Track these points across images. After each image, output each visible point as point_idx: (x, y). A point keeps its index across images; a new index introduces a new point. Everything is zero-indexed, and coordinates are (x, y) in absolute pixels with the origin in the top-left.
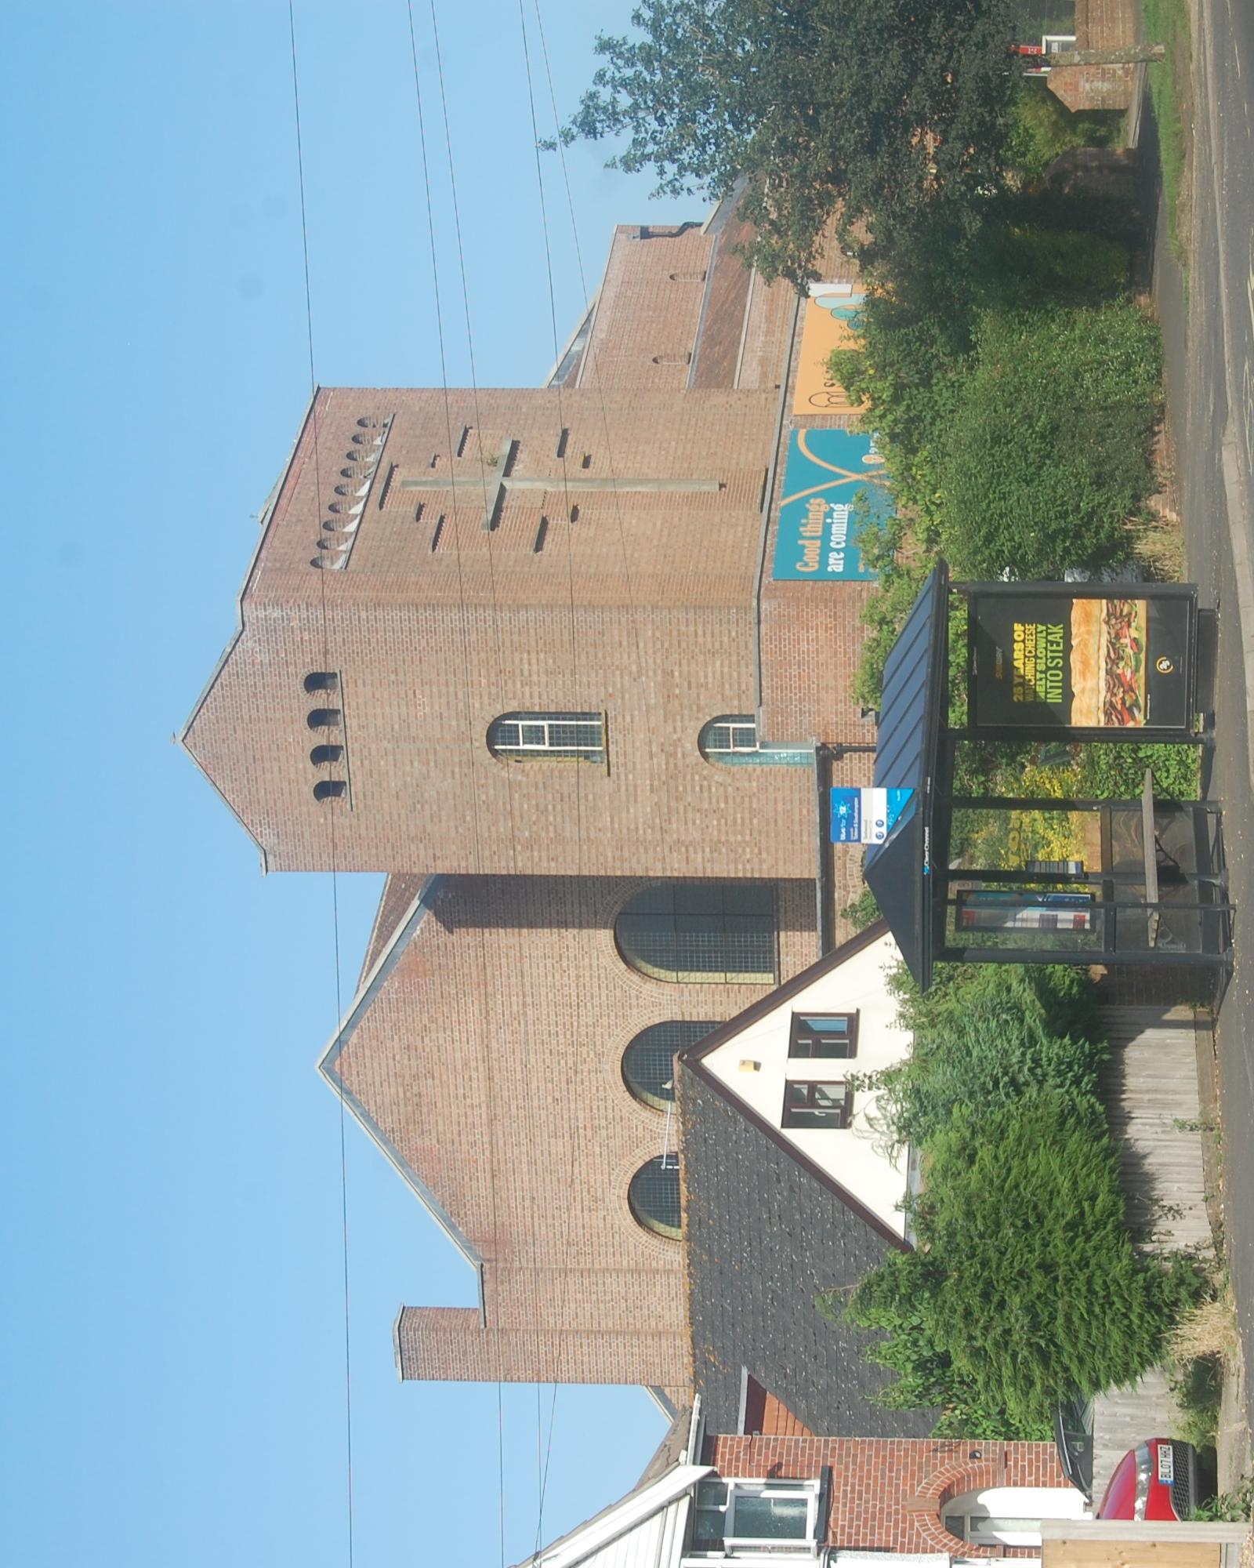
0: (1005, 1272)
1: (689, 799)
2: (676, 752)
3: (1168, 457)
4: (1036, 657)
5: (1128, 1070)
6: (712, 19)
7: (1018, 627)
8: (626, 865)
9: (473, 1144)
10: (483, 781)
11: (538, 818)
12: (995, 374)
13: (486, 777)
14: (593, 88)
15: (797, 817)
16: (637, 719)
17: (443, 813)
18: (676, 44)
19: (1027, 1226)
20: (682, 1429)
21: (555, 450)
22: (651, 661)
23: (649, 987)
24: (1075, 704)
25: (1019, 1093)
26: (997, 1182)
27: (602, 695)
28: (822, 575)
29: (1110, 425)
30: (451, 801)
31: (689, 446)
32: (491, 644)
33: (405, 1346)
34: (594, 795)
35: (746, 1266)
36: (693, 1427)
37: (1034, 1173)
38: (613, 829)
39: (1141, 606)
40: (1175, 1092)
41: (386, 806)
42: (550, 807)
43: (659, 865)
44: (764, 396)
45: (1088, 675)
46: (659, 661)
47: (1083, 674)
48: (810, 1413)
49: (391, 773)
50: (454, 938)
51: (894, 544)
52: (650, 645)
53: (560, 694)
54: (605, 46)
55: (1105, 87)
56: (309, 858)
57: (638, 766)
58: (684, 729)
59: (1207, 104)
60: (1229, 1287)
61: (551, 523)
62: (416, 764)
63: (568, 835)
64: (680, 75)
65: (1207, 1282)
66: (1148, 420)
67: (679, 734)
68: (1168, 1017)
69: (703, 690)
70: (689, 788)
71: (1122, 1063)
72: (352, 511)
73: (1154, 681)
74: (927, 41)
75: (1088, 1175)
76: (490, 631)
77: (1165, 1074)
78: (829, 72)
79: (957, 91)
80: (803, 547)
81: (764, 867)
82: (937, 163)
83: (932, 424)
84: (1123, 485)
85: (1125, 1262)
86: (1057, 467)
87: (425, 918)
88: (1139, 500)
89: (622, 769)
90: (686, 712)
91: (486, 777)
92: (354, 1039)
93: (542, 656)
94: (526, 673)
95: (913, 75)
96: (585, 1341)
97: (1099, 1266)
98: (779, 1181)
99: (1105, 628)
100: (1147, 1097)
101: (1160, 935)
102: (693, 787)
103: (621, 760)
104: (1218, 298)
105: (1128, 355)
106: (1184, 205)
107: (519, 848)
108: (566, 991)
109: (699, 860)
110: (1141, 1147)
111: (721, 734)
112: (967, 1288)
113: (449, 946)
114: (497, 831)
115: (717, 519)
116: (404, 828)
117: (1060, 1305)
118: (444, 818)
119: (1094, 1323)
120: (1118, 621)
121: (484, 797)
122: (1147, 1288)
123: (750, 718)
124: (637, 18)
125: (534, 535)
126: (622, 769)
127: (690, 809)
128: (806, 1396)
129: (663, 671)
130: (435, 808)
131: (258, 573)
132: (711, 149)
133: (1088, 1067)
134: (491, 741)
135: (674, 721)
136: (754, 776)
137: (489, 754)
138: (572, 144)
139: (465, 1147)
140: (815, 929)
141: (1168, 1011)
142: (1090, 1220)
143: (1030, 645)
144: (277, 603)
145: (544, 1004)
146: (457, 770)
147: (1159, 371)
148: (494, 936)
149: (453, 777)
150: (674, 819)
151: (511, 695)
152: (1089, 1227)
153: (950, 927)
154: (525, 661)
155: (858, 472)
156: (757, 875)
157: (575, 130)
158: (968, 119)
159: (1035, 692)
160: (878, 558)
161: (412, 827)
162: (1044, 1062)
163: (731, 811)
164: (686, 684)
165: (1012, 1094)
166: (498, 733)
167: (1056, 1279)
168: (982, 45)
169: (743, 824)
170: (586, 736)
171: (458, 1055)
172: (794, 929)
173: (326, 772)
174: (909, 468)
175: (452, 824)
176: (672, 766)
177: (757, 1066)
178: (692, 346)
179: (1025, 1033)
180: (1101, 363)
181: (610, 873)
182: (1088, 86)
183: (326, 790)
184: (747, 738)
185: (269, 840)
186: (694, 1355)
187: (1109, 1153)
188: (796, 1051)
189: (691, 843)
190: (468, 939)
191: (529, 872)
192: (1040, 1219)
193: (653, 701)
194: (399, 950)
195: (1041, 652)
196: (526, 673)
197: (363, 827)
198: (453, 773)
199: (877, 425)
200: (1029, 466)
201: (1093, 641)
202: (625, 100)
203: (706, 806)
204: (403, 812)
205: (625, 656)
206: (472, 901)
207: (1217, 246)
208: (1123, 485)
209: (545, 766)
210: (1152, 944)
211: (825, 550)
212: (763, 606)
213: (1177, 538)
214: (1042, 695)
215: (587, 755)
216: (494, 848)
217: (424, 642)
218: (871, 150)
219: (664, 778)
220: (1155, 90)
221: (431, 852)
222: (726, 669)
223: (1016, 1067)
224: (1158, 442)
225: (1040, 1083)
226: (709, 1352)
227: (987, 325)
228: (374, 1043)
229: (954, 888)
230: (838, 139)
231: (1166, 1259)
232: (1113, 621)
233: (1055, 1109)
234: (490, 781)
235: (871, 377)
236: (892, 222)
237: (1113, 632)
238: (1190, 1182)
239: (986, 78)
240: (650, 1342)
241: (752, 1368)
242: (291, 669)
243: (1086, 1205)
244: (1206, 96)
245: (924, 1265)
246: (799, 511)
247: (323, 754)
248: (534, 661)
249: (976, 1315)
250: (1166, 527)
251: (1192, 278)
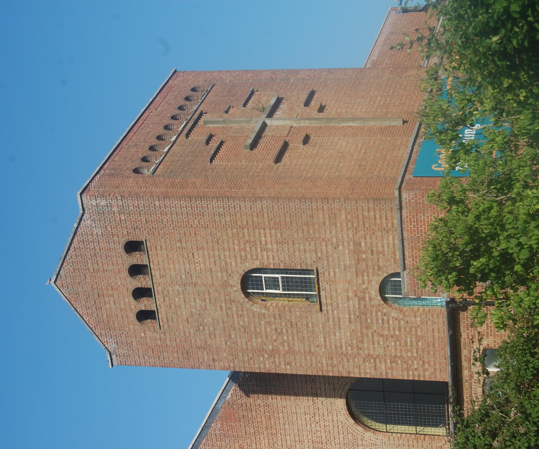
1: (375, 328)
2: (365, 297)
8: (336, 369)
10: (240, 313)
11: (277, 337)
13: (242, 311)
16: (338, 275)
17: (217, 332)
22: (345, 236)
23: (369, 434)
27: (314, 258)
30: (221, 325)
31: (388, 99)
32: (239, 223)
34: (312, 323)
38: (326, 346)
41: (181, 326)
42: (284, 331)
43: (357, 370)
46: (351, 236)
49: (183, 306)
50: (251, 400)
52: (345, 225)
53: (287, 257)
56: (137, 358)
57: (340, 306)
58: (370, 282)
62: (197, 301)
63: (297, 349)
67: (366, 285)
69: (381, 256)
70: (374, 321)
76: (238, 214)
81: (427, 373)
87: (233, 388)
89: (329, 307)
90: (371, 270)
91: (242, 311)
93: (273, 231)
94: (263, 243)
102: (377, 320)
103: (329, 301)
107: (266, 356)
108: (319, 434)
109: (383, 368)
111: (395, 285)
113: (248, 405)
114: (252, 345)
115: (399, 142)
116: (193, 341)
118: (218, 336)
121: (241, 323)
126: (329, 307)
127: (375, 334)
129: (354, 242)
130: (211, 329)
135: (363, 276)
136: (418, 314)
137: (243, 296)
145: (306, 441)
146: (223, 305)
148: (274, 400)
149: (221, 310)
150: (365, 341)
151: (255, 257)
154: (262, 235)
156: (422, 379)
161: (198, 341)
163: (403, 336)
164: (369, 251)
166: (248, 282)
169: (412, 345)
170: (306, 285)
175: (223, 339)
176: (362, 306)
181: (325, 374)
183: (144, 316)
190: (259, 401)
191: (273, 371)
193: (348, 263)
194: (219, 406)
196: (263, 243)
197: (168, 340)
198: (221, 307)
203: (386, 333)
204: (192, 330)
205: (328, 232)
206: (254, 383)
209: (280, 304)
212: (404, 195)
215: (307, 297)
217: (196, 222)
219: (357, 313)
234: (245, 313)
242: (116, 238)
247: (140, 293)
248: (268, 235)
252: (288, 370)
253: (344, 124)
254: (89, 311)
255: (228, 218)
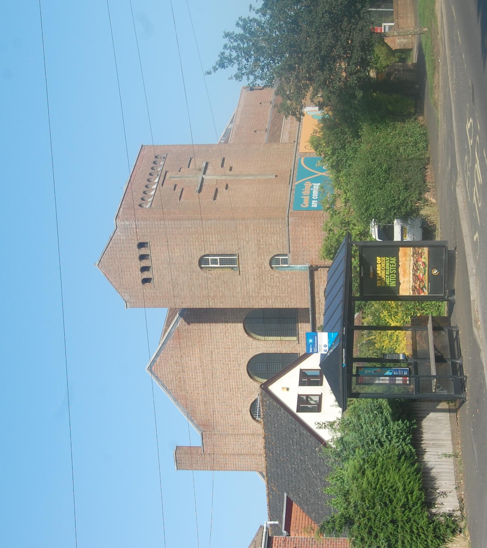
0: (377, 523)
3: (431, 178)
4: (385, 269)
5: (424, 431)
6: (264, 24)
7: (378, 258)
9: (198, 394)
12: (368, 148)
14: (223, 51)
15: (303, 288)
18: (251, 33)
19: (385, 504)
20: (260, 534)
21: (220, 165)
22: (253, 237)
23: (255, 342)
24: (401, 287)
25: (382, 446)
26: (374, 486)
28: (310, 209)
29: (410, 166)
32: (199, 232)
33: (177, 459)
35: (285, 459)
36: (264, 534)
37: (388, 481)
39: (426, 250)
40: (442, 440)
43: (257, 304)
44: (290, 145)
45: (406, 276)
47: (404, 275)
48: (308, 511)
51: (333, 203)
54: (227, 35)
55: (405, 41)
56: (140, 303)
58: (264, 259)
59: (445, 52)
60: (466, 528)
61: (219, 190)
64: (253, 44)
65: (457, 525)
66: (423, 164)
68: (438, 407)
71: (421, 427)
72: (153, 187)
73: (431, 277)
74: (342, 29)
75: (410, 482)
77: (438, 431)
78: (306, 41)
79: (353, 47)
80: (303, 198)
81: (293, 304)
82: (346, 73)
83: (346, 162)
84: (415, 189)
85: (425, 520)
86: (391, 183)
88: (421, 195)
92: (158, 360)
95: (337, 41)
96: (237, 457)
97: (415, 521)
98: (296, 431)
99: (412, 258)
100: (432, 442)
101: (437, 387)
104: (452, 127)
105: (416, 140)
106: (436, 86)
107: (210, 299)
110: (430, 465)
112: (362, 529)
117: (399, 536)
119: (413, 543)
120: (417, 255)
122: (434, 530)
123: (286, 255)
124: (238, 24)
125: (213, 194)
128: (307, 505)
131: (121, 209)
132: (266, 70)
133: (408, 433)
134: (200, 264)
137: (199, 268)
138: (217, 71)
139: (196, 395)
140: (309, 322)
141: (438, 405)
142: (411, 503)
143: (383, 265)
144: (127, 220)
147: (427, 145)
152: (411, 505)
153: (353, 386)
155: (322, 172)
156: (290, 307)
157: (217, 67)
158: (357, 57)
159: (385, 282)
160: (328, 208)
162: (392, 433)
164: (265, 244)
165: (379, 446)
166: (202, 261)
167: (398, 526)
168: (361, 30)
170: (232, 262)
171: (193, 365)
172: (303, 322)
173: (146, 275)
174: (338, 177)
177: (288, 389)
178: (267, 126)
179: (384, 420)
180: (406, 143)
181: (241, 307)
182: (399, 41)
183: (146, 281)
184: (285, 261)
185: (127, 298)
186: (268, 487)
187: (418, 471)
188: (302, 383)
189: (268, 297)
190: (195, 327)
191: (214, 307)
192: (391, 501)
194: (172, 331)
195: (387, 268)
199: (326, 162)
200: (380, 183)
201: (407, 263)
202: (234, 54)
203: (272, 284)
206: (194, 316)
207: (451, 106)
208: (415, 189)
209: (218, 272)
210: (434, 391)
211: (311, 199)
212: (290, 219)
213: (435, 209)
214: (388, 284)
215: (232, 268)
216: (202, 299)
217: (177, 232)
218: (321, 68)
220: (424, 43)
221: (181, 301)
222: (278, 239)
223: (380, 435)
224: (427, 172)
225: (390, 441)
226: (274, 487)
227: (365, 128)
228: (165, 361)
229: (355, 365)
230: (310, 65)
231: (441, 516)
232: (415, 256)
233: (396, 453)
235: (324, 146)
236: (330, 95)
237: (415, 260)
238: (450, 480)
239: (363, 42)
240: (258, 458)
241: (288, 493)
242: (133, 241)
243: (409, 496)
244: (445, 48)
245: (345, 518)
246: (302, 186)
249: (366, 539)
250: (432, 205)
251: (440, 115)
252: (222, 306)
253: (244, 178)
254: (116, 280)
255: (193, 229)
